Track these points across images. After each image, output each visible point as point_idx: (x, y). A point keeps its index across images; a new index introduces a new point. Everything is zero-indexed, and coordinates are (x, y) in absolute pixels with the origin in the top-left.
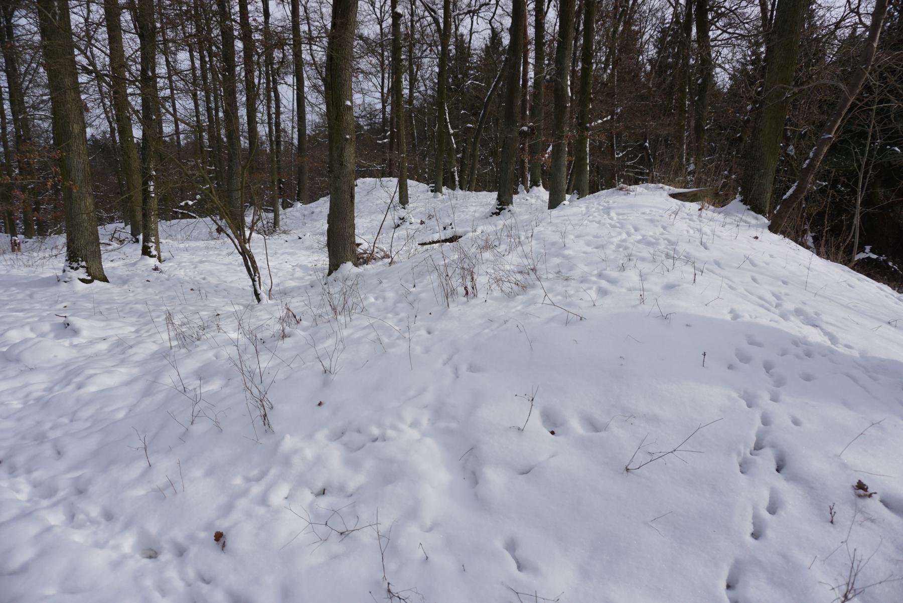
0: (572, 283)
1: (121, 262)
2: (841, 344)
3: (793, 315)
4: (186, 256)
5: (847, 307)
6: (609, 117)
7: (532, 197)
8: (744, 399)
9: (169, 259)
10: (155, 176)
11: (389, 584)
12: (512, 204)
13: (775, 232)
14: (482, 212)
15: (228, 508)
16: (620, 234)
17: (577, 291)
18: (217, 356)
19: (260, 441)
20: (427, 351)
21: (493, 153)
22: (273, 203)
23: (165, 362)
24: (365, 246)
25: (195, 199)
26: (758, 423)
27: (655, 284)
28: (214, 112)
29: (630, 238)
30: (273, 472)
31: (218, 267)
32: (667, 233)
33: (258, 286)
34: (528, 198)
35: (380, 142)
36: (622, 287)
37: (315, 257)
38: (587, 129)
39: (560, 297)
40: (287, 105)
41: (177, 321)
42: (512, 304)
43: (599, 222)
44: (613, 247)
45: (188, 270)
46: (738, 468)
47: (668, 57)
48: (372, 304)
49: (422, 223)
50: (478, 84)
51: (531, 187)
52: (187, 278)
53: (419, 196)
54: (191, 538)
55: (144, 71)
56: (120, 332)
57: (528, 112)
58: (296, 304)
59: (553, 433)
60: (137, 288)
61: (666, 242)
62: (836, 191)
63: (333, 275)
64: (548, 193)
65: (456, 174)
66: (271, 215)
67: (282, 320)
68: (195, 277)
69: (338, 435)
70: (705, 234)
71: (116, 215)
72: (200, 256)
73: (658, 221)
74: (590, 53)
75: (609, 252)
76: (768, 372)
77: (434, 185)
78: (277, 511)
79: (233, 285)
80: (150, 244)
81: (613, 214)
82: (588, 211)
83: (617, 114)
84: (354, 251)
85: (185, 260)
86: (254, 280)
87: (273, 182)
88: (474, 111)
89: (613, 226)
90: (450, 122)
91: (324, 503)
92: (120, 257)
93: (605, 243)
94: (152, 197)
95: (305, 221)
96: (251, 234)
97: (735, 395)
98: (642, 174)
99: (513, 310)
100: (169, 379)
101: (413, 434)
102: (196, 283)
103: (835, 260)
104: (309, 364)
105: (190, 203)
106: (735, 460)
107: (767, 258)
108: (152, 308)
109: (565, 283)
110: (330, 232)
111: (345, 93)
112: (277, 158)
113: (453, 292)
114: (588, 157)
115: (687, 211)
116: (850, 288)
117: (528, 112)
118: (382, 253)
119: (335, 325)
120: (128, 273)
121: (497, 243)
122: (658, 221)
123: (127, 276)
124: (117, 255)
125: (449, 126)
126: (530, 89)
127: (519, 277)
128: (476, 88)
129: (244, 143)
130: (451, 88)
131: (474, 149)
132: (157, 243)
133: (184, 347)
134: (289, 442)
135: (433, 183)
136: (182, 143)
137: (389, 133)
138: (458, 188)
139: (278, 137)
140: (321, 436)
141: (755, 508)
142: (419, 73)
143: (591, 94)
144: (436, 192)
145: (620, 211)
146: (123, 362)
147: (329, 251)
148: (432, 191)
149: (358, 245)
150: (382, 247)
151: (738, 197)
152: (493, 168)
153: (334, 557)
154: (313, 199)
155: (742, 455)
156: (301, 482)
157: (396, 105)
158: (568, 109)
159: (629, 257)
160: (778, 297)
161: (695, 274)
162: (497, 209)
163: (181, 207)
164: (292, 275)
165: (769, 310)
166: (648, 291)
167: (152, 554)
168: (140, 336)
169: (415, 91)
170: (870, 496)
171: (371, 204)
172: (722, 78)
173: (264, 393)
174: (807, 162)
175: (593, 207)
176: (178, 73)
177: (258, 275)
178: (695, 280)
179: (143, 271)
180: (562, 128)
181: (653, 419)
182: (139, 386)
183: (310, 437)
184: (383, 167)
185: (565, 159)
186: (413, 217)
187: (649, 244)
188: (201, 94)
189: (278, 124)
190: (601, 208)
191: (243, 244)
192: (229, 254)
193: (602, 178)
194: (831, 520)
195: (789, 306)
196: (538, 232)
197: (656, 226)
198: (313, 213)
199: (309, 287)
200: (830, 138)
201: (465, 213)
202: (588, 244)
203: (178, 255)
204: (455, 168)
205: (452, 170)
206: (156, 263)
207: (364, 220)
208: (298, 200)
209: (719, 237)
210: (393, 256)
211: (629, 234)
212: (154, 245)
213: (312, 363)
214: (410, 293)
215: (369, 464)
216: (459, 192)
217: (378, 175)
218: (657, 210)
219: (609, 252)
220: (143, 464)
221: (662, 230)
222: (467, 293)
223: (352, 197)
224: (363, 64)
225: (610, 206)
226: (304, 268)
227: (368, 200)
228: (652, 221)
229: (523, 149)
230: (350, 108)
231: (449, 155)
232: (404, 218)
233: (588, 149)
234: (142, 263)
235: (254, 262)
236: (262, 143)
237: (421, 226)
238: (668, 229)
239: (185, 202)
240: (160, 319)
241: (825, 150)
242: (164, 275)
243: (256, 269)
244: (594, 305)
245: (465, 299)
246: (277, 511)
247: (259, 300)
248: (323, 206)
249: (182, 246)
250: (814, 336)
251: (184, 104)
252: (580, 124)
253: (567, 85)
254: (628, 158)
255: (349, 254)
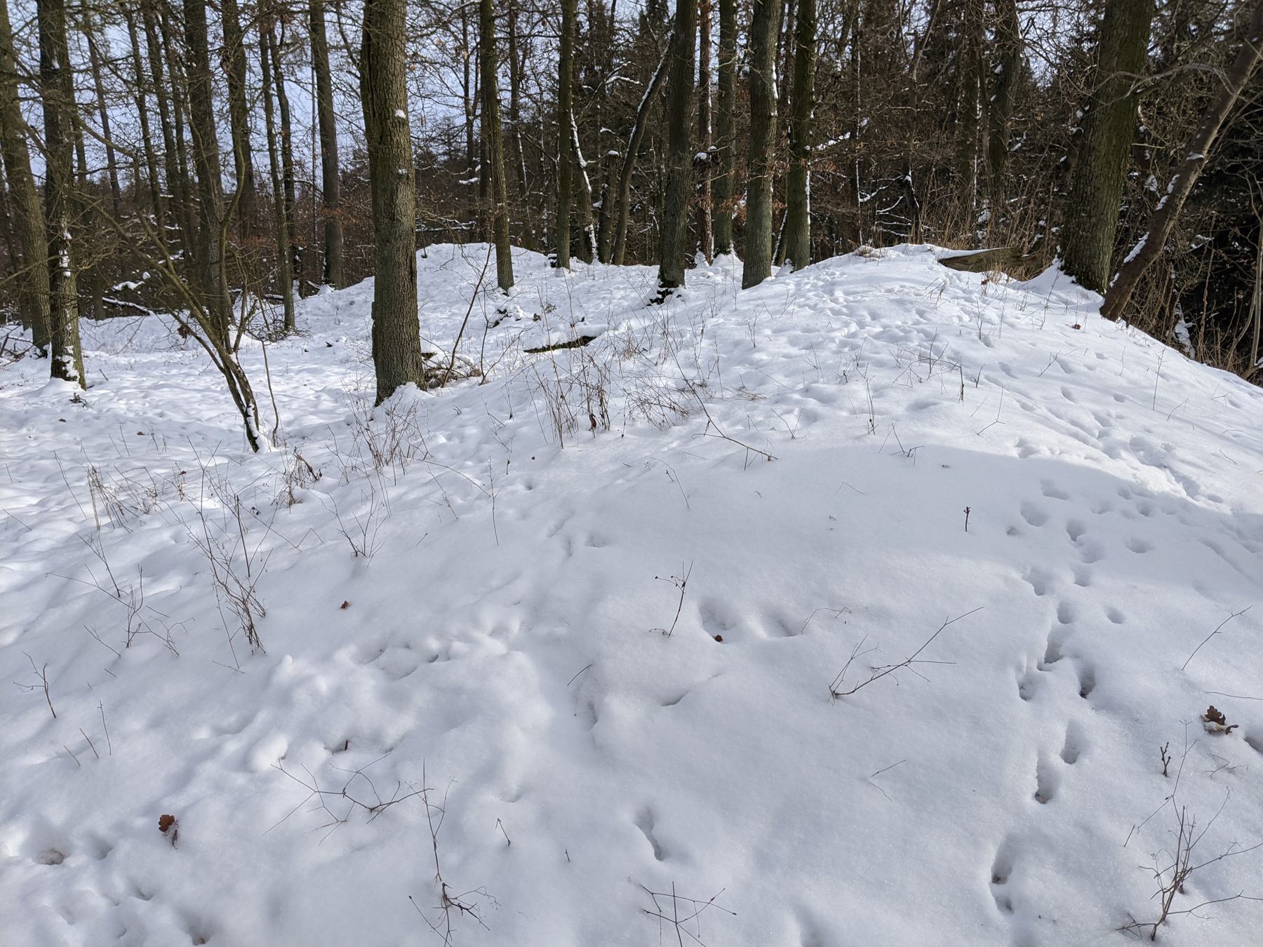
0: (761, 405)
1: (17, 390)
2: (1204, 496)
3: (1126, 449)
4: (130, 378)
5: (1221, 437)
6: (848, 136)
7: (716, 273)
8: (1031, 582)
9: (100, 383)
10: (70, 241)
11: (444, 885)
12: (683, 284)
13: (1112, 318)
14: (635, 298)
15: (183, 779)
16: (847, 325)
17: (768, 417)
18: (177, 538)
19: (242, 669)
20: (524, 516)
21: (655, 200)
22: (283, 289)
23: (88, 550)
24: (440, 356)
25: (141, 279)
26: (1052, 620)
27: (896, 403)
28: (175, 131)
29: (862, 330)
30: (262, 717)
31: (185, 396)
32: (925, 321)
33: (253, 425)
34: (711, 274)
35: (464, 182)
36: (841, 409)
37: (353, 376)
38: (807, 154)
39: (740, 427)
40: (301, 119)
41: (111, 484)
42: (665, 439)
43: (814, 307)
44: (833, 346)
45: (132, 402)
46: (1017, 691)
47: (947, 30)
48: (442, 446)
49: (536, 318)
50: (628, 82)
51: (715, 256)
52: (131, 415)
53: (531, 274)
54: (122, 828)
55: (45, 61)
56: (13, 505)
57: (710, 128)
58: (315, 452)
59: (719, 639)
60: (44, 432)
61: (922, 335)
62: (1227, 252)
63: (387, 403)
64: (743, 263)
65: (592, 235)
66: (280, 309)
67: (290, 478)
68: (145, 413)
69: (372, 655)
70: (989, 322)
71: (8, 312)
72: (154, 377)
73: (912, 303)
74: (810, 24)
75: (826, 355)
76: (1074, 539)
77: (555, 255)
78: (267, 779)
79: (212, 425)
80: (65, 359)
81: (839, 294)
82: (799, 290)
83: (861, 129)
84: (418, 365)
85: (127, 384)
86: (246, 415)
87: (281, 251)
88: (621, 127)
89: (836, 313)
90: (581, 147)
91: (344, 764)
92: (15, 381)
93: (820, 339)
94: (66, 277)
95: (340, 317)
96: (239, 337)
97: (1016, 575)
98: (898, 228)
99: (666, 449)
100: (93, 578)
101: (497, 646)
102: (147, 422)
103: (1222, 365)
104: (330, 543)
105: (132, 286)
106: (1013, 679)
107: (1091, 359)
108: (66, 465)
109: (751, 404)
110: (377, 334)
111: (395, 96)
112: (287, 210)
113: (572, 424)
114: (808, 201)
115: (963, 285)
116: (1233, 407)
117: (710, 128)
118: (468, 367)
119: (375, 481)
120: (27, 407)
121: (647, 346)
122: (912, 303)
123: (26, 412)
124: (8, 379)
125: (580, 153)
126: (713, 89)
127: (676, 397)
128: (626, 88)
129: (228, 183)
130: (582, 90)
131: (622, 193)
132: (78, 355)
133: (121, 525)
134: (290, 667)
135: (555, 252)
136: (121, 185)
137: (479, 167)
138: (596, 260)
139: (288, 174)
140: (345, 656)
141: (1042, 754)
142: (527, 62)
143: (812, 94)
144: (559, 266)
145: (851, 288)
146: (15, 554)
147: (376, 365)
148: (553, 265)
149: (429, 356)
150: (467, 357)
151: (1056, 262)
152: (655, 225)
153: (359, 848)
154: (353, 280)
155: (1025, 670)
156: (309, 731)
157: (490, 119)
158: (774, 121)
159: (858, 362)
160: (1103, 422)
161: (963, 385)
162: (659, 292)
163: (115, 294)
164: (315, 406)
165: (1085, 442)
166: (881, 413)
167: (56, 857)
168: (46, 511)
169: (522, 95)
170: (1228, 731)
171: (451, 288)
172: (1040, 68)
173: (248, 590)
174: (1164, 199)
175: (807, 284)
176: (110, 62)
177: (253, 406)
178: (962, 393)
179: (53, 403)
180: (764, 153)
181: (879, 615)
182: (41, 592)
183: (325, 658)
184: (472, 225)
185: (770, 206)
186: (521, 308)
187: (894, 339)
188: (151, 101)
189: (287, 152)
190: (821, 283)
191: (226, 353)
192: (205, 372)
193: (837, 238)
194: (1163, 770)
195: (1121, 434)
196: (715, 326)
197: (909, 311)
198: (352, 303)
199: (344, 425)
200: (1201, 160)
201: (607, 302)
202: (793, 342)
203: (116, 377)
204: (592, 226)
205: (586, 229)
206: (76, 391)
207: (439, 315)
208: (327, 282)
209: (1012, 326)
210: (485, 372)
211: (861, 325)
212: (72, 360)
213: (335, 542)
214: (503, 427)
215: (422, 697)
216: (597, 266)
217: (457, 239)
218: (914, 285)
219: (826, 355)
220: (43, 714)
221: (917, 317)
222: (594, 424)
223: (413, 273)
224: (429, 50)
225: (836, 279)
226: (337, 395)
227: (445, 281)
228: (900, 302)
229: (702, 191)
230: (404, 123)
231: (581, 203)
232: (505, 311)
233: (808, 189)
234: (52, 390)
235: (245, 385)
236: (263, 185)
237: (535, 323)
238: (926, 315)
239: (124, 284)
240: (83, 484)
241: (1193, 179)
242: (90, 410)
243: (249, 396)
244: (793, 437)
245: (591, 433)
246: (267, 779)
247: (256, 448)
248: (364, 291)
249: (123, 360)
250: (1159, 482)
251: (123, 117)
252: (793, 147)
253: (771, 80)
254: (881, 202)
255: (410, 369)
